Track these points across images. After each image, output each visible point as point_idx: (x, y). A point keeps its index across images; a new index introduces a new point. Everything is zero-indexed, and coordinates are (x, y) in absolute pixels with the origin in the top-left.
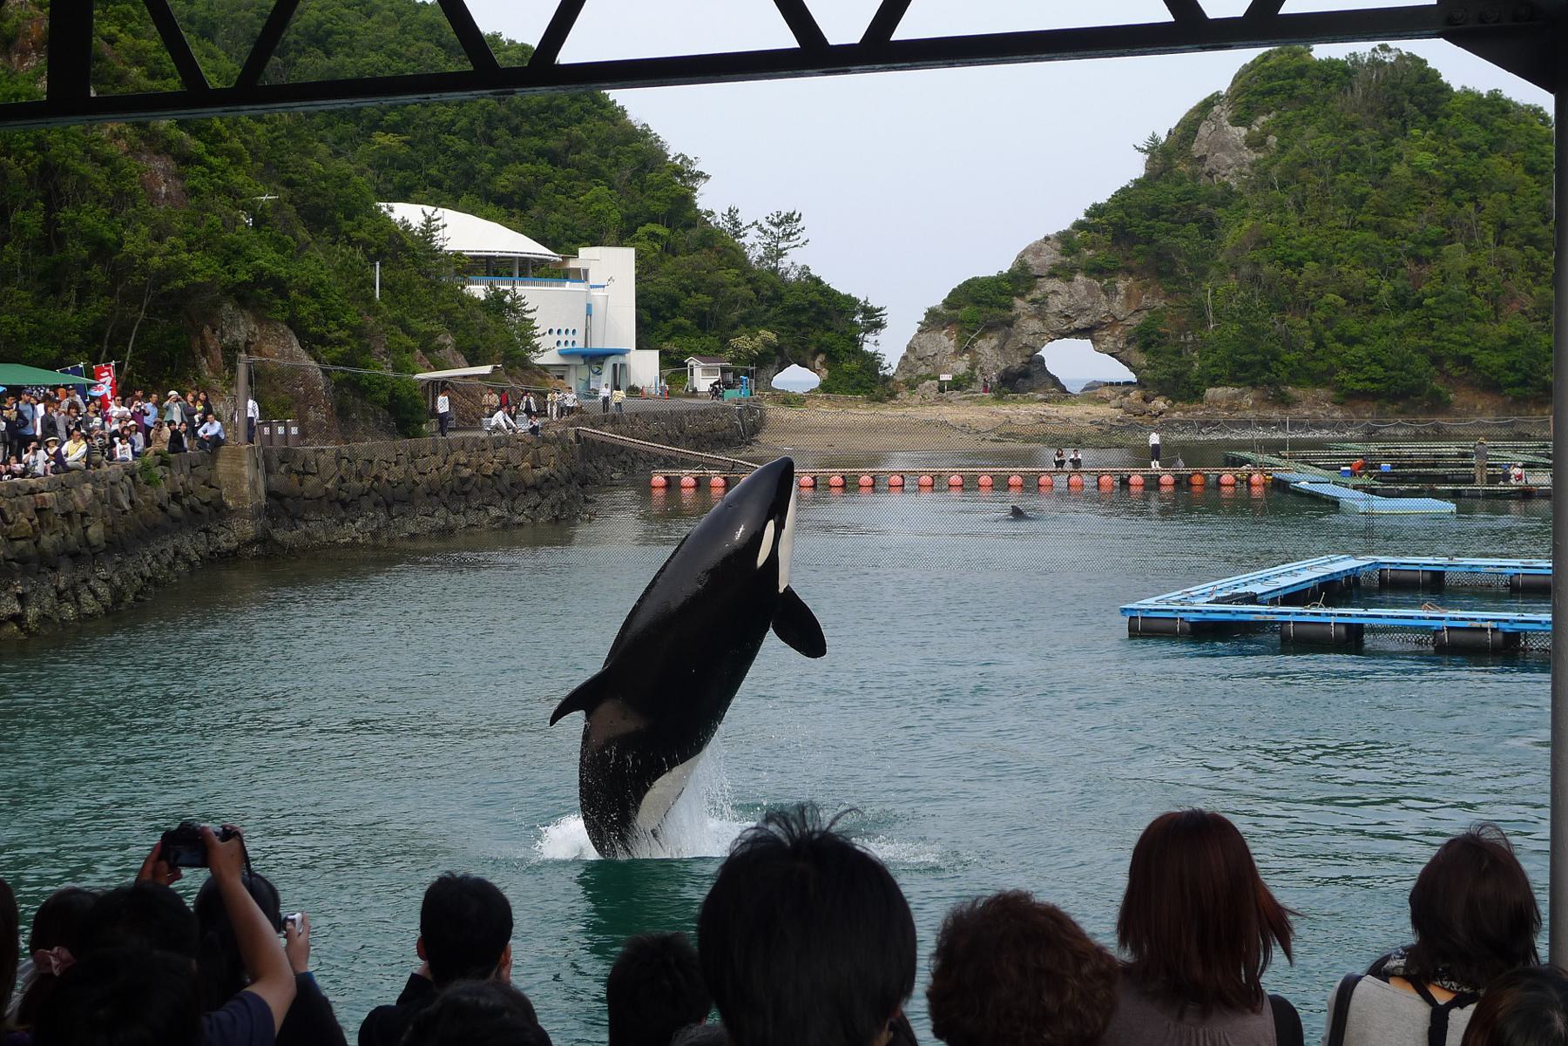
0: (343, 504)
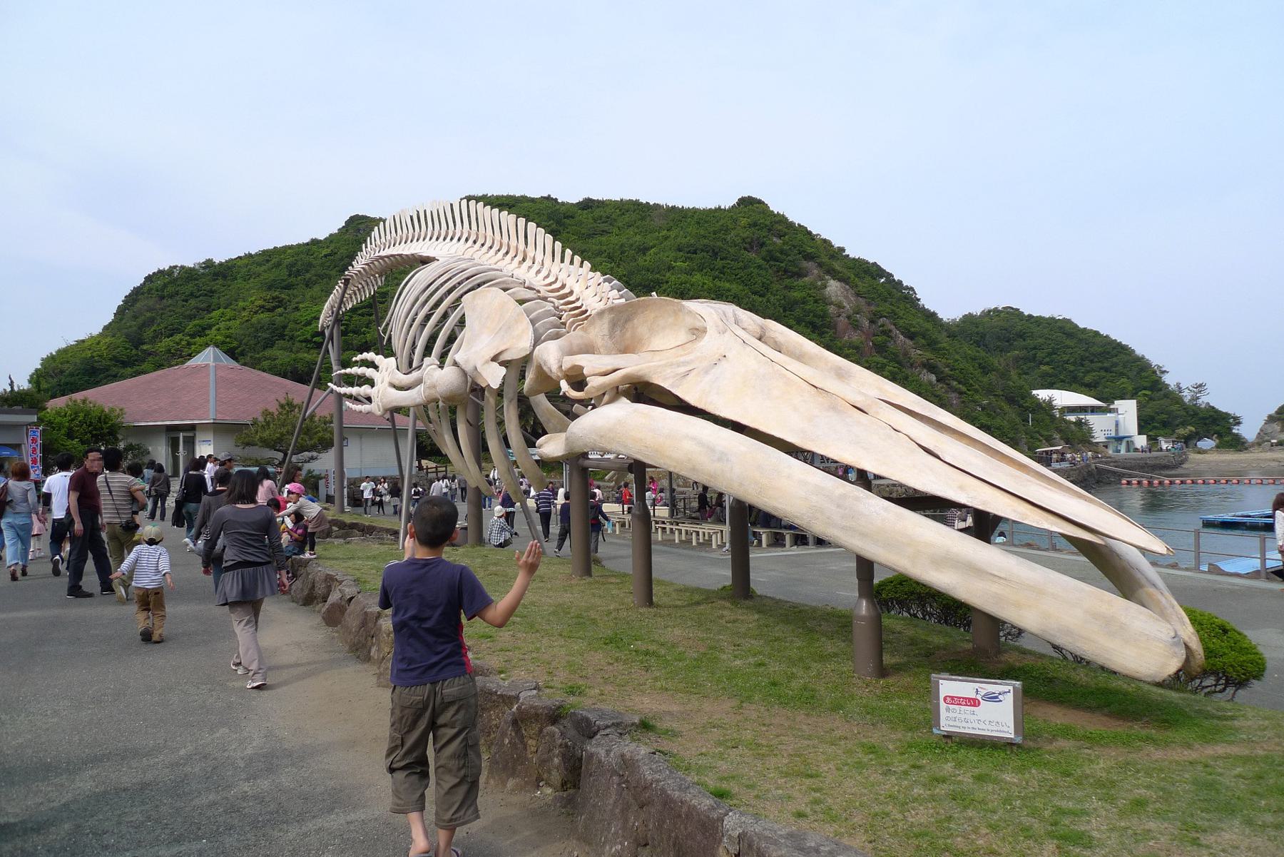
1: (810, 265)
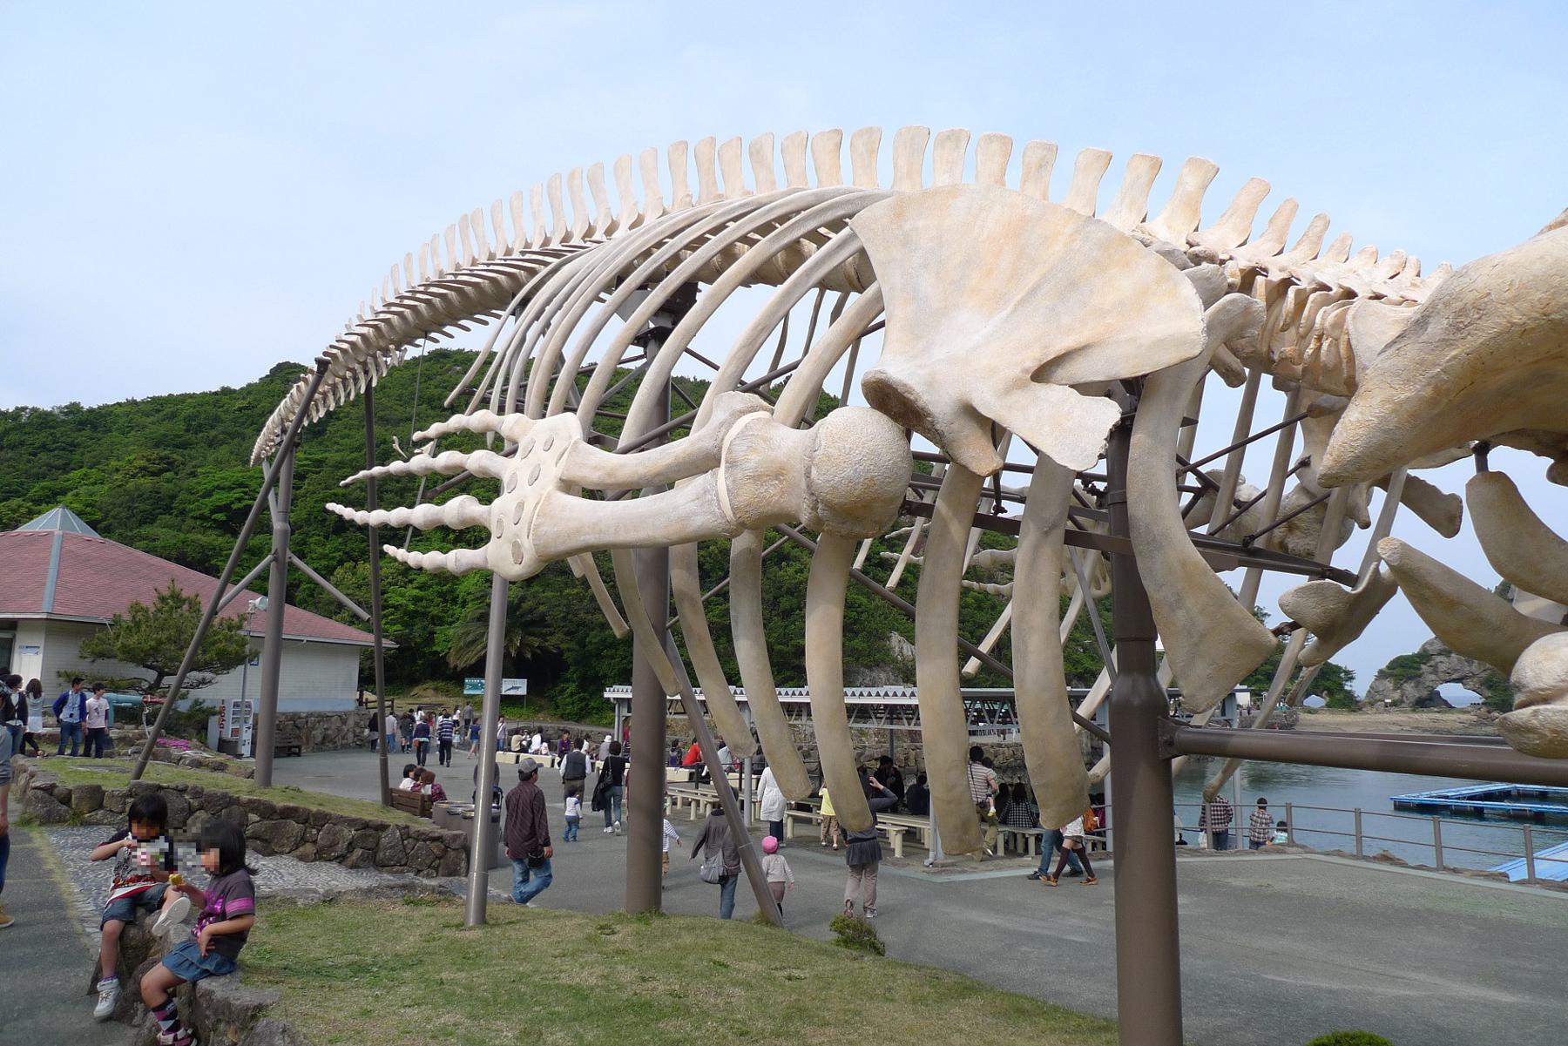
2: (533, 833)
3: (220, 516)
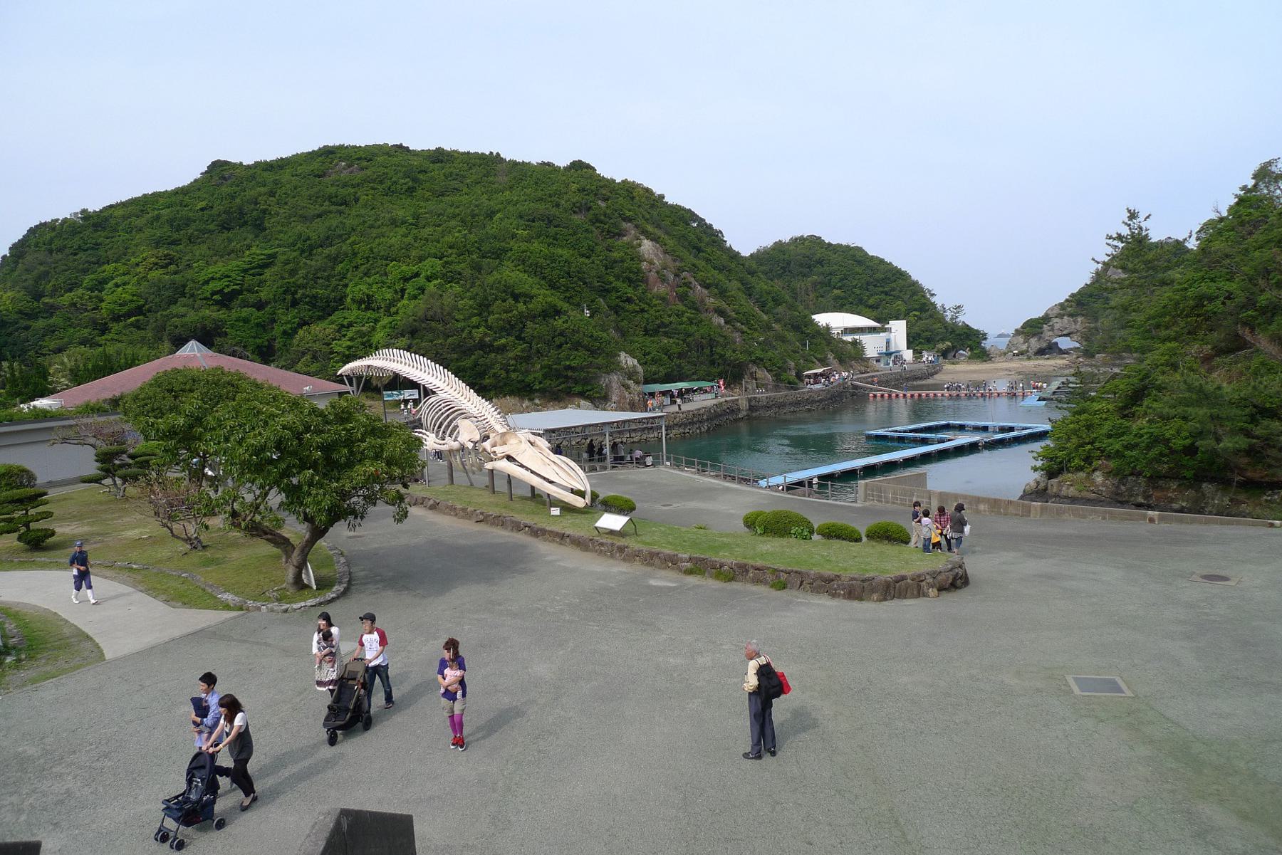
0: (768, 407)
1: (625, 225)
2: (895, 539)
3: (217, 297)
